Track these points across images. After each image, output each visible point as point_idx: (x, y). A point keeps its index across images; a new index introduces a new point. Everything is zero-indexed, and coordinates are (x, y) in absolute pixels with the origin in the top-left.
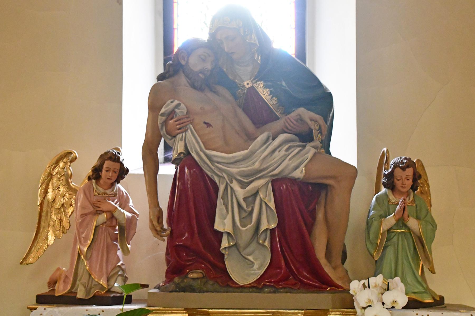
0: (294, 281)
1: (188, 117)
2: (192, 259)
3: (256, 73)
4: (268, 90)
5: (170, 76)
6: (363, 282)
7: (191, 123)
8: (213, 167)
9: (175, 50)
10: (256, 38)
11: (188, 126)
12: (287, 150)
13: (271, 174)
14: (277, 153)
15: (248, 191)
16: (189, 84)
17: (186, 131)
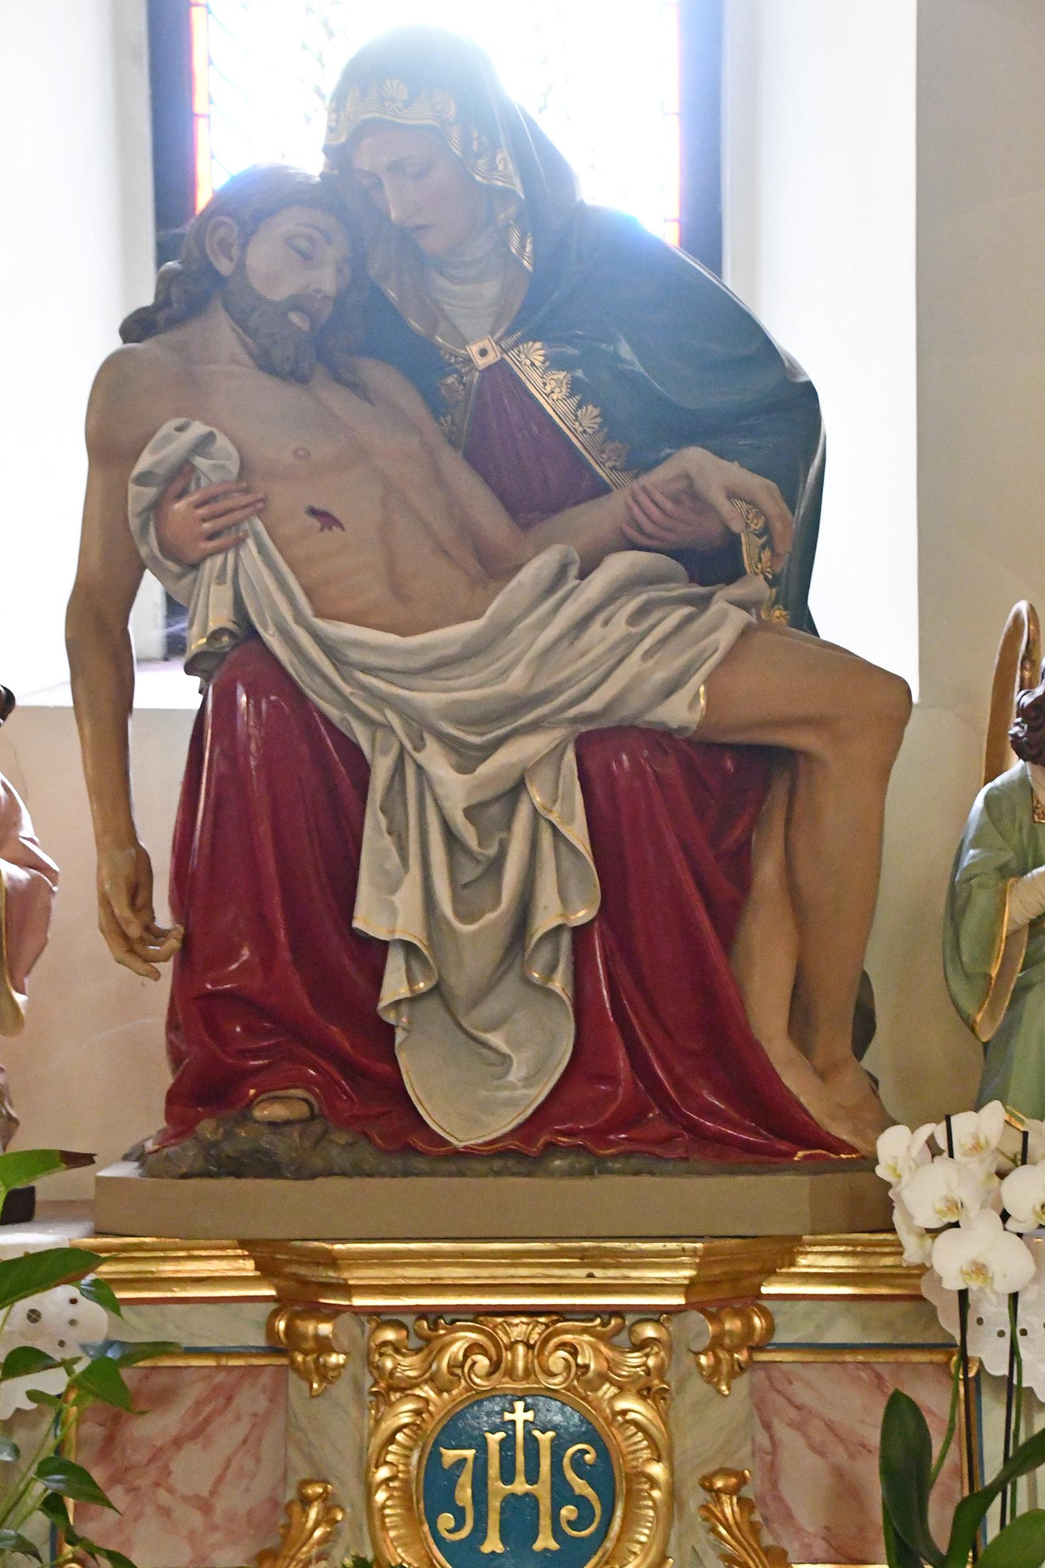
0: (665, 1129)
1: (247, 491)
2: (267, 1048)
3: (516, 308)
4: (561, 375)
5: (174, 322)
6: (925, 1131)
7: (259, 513)
8: (346, 689)
9: (203, 200)
10: (511, 166)
11: (246, 526)
12: (633, 619)
13: (572, 713)
14: (595, 628)
15: (488, 780)
16: (251, 355)
17: (239, 543)
